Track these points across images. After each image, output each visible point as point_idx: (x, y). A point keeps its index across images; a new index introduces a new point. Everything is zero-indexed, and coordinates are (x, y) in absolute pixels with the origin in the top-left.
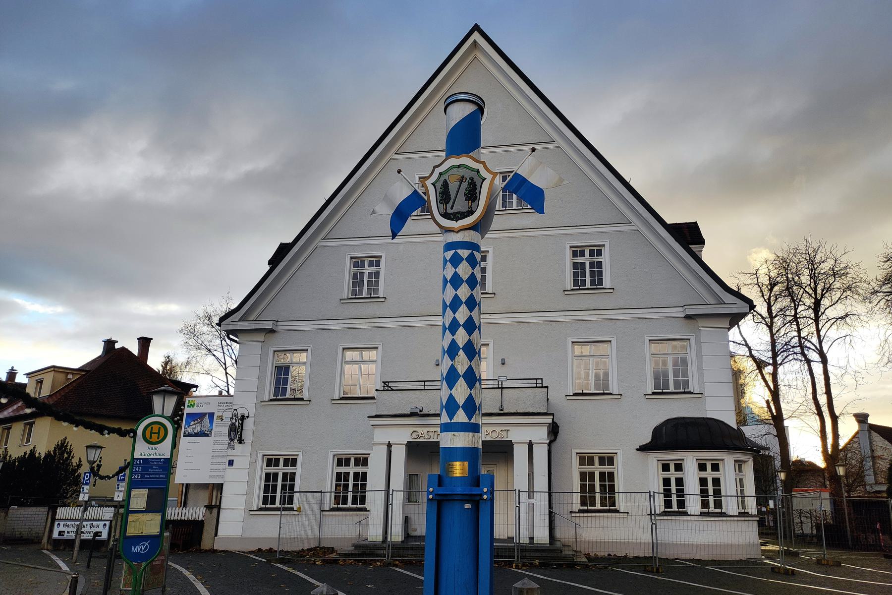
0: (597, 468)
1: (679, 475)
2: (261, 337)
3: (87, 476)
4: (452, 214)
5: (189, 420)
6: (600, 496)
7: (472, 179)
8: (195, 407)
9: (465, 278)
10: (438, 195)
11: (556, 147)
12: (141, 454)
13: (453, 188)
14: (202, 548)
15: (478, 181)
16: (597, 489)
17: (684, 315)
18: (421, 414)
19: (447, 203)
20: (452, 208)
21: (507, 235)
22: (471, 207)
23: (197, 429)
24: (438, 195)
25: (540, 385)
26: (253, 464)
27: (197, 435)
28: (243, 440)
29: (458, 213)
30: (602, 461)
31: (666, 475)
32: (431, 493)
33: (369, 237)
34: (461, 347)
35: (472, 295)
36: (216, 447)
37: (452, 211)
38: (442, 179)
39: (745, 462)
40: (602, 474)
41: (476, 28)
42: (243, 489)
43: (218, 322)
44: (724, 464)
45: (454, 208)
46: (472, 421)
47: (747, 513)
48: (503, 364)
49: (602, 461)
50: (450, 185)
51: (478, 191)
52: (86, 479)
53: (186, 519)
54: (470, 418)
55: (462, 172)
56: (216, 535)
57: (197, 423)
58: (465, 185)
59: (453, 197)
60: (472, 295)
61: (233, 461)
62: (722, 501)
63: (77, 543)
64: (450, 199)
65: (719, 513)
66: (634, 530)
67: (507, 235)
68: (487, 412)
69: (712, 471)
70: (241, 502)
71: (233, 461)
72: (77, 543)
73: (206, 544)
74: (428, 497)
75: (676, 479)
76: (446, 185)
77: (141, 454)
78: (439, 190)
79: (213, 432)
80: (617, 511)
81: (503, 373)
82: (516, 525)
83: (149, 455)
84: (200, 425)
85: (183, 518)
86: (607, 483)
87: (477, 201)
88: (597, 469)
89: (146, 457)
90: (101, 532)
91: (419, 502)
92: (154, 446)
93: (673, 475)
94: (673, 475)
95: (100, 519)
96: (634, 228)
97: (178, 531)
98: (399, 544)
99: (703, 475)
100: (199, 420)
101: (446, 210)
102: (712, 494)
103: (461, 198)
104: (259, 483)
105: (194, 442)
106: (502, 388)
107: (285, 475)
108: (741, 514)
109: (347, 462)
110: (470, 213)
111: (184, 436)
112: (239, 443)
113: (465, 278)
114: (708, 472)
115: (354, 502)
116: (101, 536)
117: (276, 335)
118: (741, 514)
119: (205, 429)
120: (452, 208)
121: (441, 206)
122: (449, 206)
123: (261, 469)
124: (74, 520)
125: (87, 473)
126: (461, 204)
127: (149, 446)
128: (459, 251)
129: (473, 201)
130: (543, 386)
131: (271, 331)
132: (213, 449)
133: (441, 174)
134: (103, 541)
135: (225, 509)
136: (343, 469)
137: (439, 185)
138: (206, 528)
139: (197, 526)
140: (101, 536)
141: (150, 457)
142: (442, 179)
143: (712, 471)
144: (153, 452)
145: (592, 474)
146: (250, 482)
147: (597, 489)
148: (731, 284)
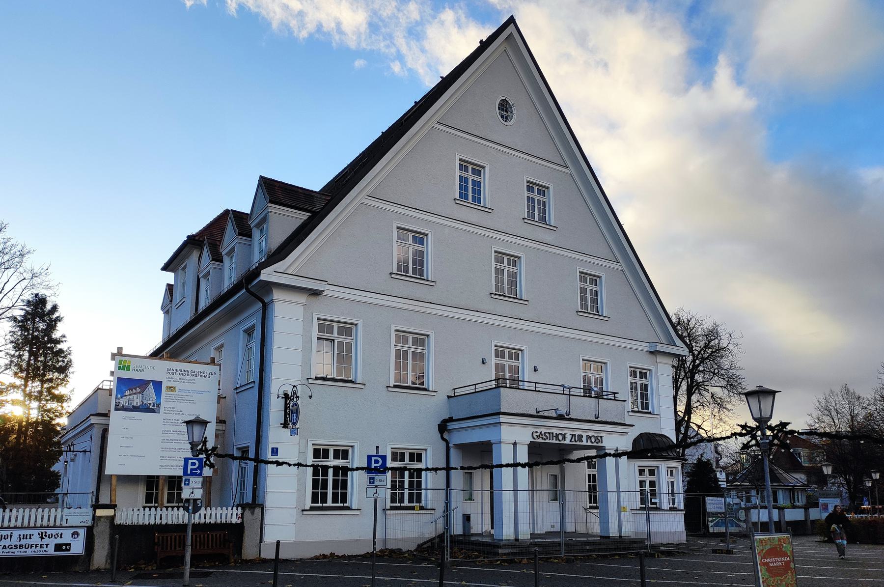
2: (302, 299)
5: (123, 388)
6: (409, 493)
8: (131, 369)
11: (567, 173)
14: (244, 557)
16: (406, 485)
17: (29, 263)
18: (538, 416)
21: (535, 246)
23: (137, 401)
27: (136, 409)
30: (412, 458)
31: (642, 478)
33: (507, 233)
36: (167, 428)
47: (676, 508)
48: (484, 363)
49: (337, 454)
52: (190, 467)
53: (213, 522)
56: (261, 541)
57: (136, 393)
62: (328, 493)
64: (74, 532)
65: (654, 508)
66: (678, 523)
67: (535, 246)
68: (587, 419)
71: (277, 449)
73: (249, 551)
75: (671, 482)
79: (162, 407)
80: (348, 508)
81: (535, 378)
82: (647, 521)
84: (140, 396)
85: (208, 521)
86: (415, 480)
88: (331, 462)
90: (70, 544)
91: (474, 500)
93: (647, 478)
94: (647, 478)
95: (58, 524)
96: (620, 268)
97: (206, 539)
98: (617, 539)
99: (642, 478)
100: (138, 390)
102: (489, 489)
105: (133, 418)
106: (570, 395)
108: (671, 509)
111: (116, 409)
112: (283, 427)
115: (335, 500)
116: (69, 550)
117: (319, 299)
118: (671, 509)
119: (149, 402)
124: (25, 528)
131: (315, 293)
132: (163, 431)
134: (75, 558)
135: (272, 509)
138: (247, 533)
139: (235, 532)
140: (69, 550)
145: (325, 468)
147: (406, 485)
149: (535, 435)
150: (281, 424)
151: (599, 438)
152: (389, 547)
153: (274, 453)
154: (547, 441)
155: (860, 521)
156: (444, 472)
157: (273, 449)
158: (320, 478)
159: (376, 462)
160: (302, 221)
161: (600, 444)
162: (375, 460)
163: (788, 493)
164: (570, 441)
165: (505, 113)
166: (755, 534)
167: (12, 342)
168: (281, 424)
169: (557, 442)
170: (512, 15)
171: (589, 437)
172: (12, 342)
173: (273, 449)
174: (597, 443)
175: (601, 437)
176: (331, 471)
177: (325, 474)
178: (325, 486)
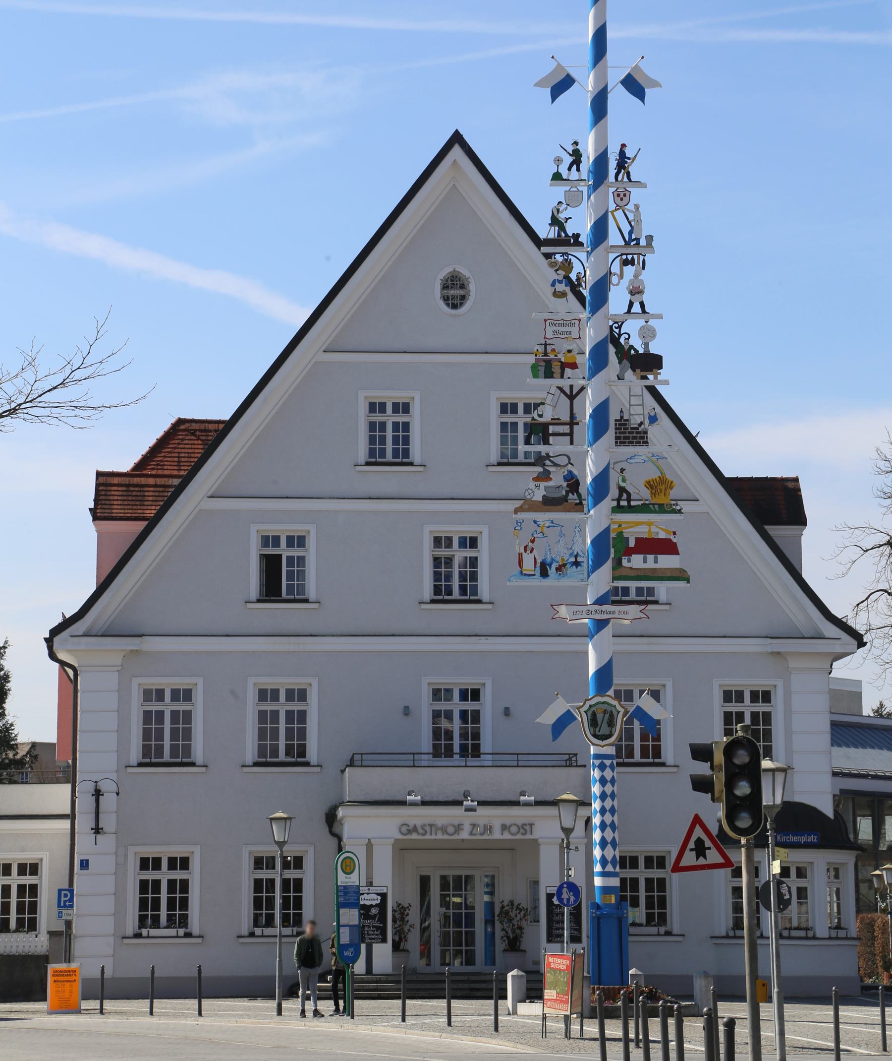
0: (642, 872)
1: (802, 883)
4: (599, 735)
7: (611, 712)
10: (589, 720)
13: (599, 717)
15: (615, 713)
19: (596, 727)
20: (599, 732)
22: (611, 732)
24: (589, 720)
25: (575, 764)
28: (102, 829)
29: (604, 735)
32: (594, 913)
34: (608, 824)
40: (172, 883)
41: (457, 139)
43: (48, 636)
44: (812, 870)
45: (601, 731)
50: (597, 715)
51: (615, 720)
52: (63, 899)
54: (615, 870)
55: (605, 707)
58: (607, 716)
59: (599, 723)
61: (87, 861)
63: (838, 902)
64: (598, 725)
69: (797, 878)
70: (108, 925)
71: (87, 861)
72: (838, 902)
74: (592, 915)
76: (594, 715)
83: (347, 883)
86: (656, 894)
87: (615, 728)
89: (345, 884)
92: (348, 876)
101: (595, 732)
102: (492, 1002)
103: (605, 725)
114: (791, 879)
120: (599, 732)
121: (591, 728)
122: (597, 730)
123: (134, 876)
125: (65, 890)
126: (605, 730)
127: (346, 875)
128: (604, 761)
130: (578, 765)
133: (591, 706)
137: (590, 713)
141: (347, 884)
143: (797, 878)
144: (348, 880)
145: (157, 884)
146: (119, 894)
148: (838, 613)
149: (404, 829)
150: (92, 829)
151: (528, 828)
152: (273, 1004)
153: (84, 866)
154: (428, 837)
156: (621, 1045)
157: (82, 861)
159: (66, 896)
160: (144, 526)
161: (528, 836)
162: (64, 894)
164: (471, 834)
166: (629, 1018)
167: (37, 761)
168: (103, 795)
169: (446, 837)
170: (457, 129)
171: (504, 828)
172: (37, 761)
174: (523, 834)
175: (531, 825)
177: (170, 918)
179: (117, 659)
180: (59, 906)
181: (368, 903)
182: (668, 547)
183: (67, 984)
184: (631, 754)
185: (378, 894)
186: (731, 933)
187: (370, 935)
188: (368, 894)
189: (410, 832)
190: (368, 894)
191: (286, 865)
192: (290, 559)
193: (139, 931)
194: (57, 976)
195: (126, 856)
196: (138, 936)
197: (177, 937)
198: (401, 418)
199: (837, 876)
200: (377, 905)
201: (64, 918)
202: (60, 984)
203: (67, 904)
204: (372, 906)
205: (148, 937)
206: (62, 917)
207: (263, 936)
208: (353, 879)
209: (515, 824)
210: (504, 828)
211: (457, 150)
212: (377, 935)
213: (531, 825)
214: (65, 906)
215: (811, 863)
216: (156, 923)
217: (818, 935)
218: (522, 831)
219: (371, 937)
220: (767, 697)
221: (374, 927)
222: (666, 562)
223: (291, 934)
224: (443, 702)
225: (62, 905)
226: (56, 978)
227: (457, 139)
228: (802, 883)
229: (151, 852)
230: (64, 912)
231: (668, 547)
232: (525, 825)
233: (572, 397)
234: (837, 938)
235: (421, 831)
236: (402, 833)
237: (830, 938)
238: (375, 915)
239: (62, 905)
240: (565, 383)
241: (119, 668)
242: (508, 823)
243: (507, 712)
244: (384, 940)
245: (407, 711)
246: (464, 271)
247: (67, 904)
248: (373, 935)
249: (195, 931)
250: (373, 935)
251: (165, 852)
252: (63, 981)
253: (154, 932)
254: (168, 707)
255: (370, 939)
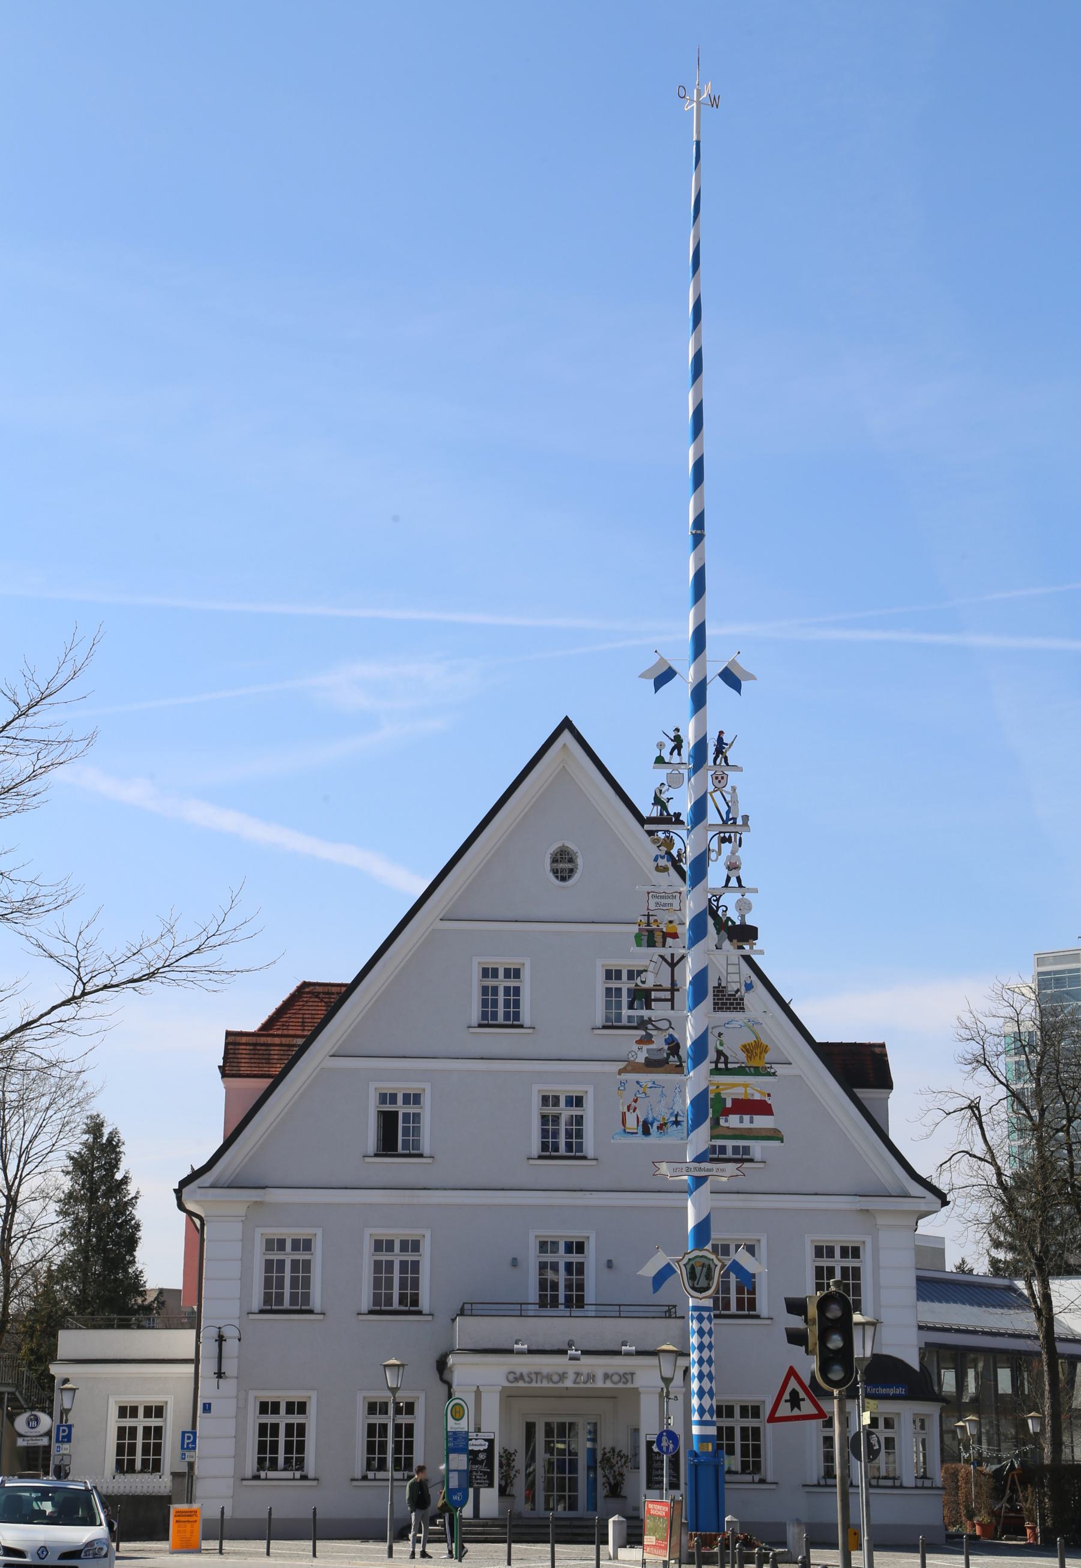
1: (889, 1433)
3: (189, 1438)
7: (709, 1265)
9: (706, 1344)
12: (451, 1428)
13: (698, 1270)
15: (712, 1266)
16: (390, 1446)
22: (709, 1284)
26: (241, 1410)
28: (224, 1373)
29: (702, 1288)
35: (702, 1342)
37: (698, 1286)
38: (691, 1263)
39: (928, 1415)
41: (566, 724)
42: (228, 1447)
46: (703, 1419)
49: (570, 1101)
52: (186, 1441)
55: (703, 1260)
58: (705, 1269)
59: (698, 1276)
60: (702, 1342)
61: (210, 1404)
62: (142, 1438)
70: (228, 1467)
71: (210, 1404)
76: (693, 1268)
77: (451, 1428)
78: (688, 1271)
92: (457, 1422)
103: (703, 1278)
104: (252, 1439)
107: (289, 1427)
109: (384, 1409)
110: (708, 1288)
113: (706, 1344)
122: (696, 1282)
123: (253, 1420)
125: (189, 1432)
126: (703, 1283)
129: (710, 1280)
136: (377, 1419)
137: (689, 1267)
142: (691, 1263)
145: (275, 1427)
146: (239, 1437)
147: (390, 1446)
150: (215, 1373)
151: (629, 1377)
152: (384, 1546)
154: (533, 1385)
155: (868, 1536)
157: (204, 1404)
158: (268, 1439)
159: (189, 1438)
161: (629, 1385)
163: (854, 1484)
165: (116, 1322)
169: (551, 1385)
170: (567, 717)
171: (607, 1376)
173: (204, 1404)
174: (624, 1383)
175: (632, 1374)
176: (138, 1465)
178: (289, 1447)
179: (242, 1210)
180: (182, 1448)
181: (476, 1448)
182: (762, 1108)
183: (189, 1525)
184: (727, 1306)
185: (485, 1440)
186: (822, 1482)
187: (476, 1479)
188: (476, 1439)
189: (516, 1380)
190: (476, 1439)
191: (398, 1411)
192: (406, 1116)
193: (257, 1473)
194: (179, 1516)
195: (246, 1400)
196: (256, 1478)
197: (294, 1479)
198: (296, 1419)
199: (923, 1427)
200: (484, 1451)
201: (187, 1459)
202: (181, 1524)
203: (190, 1446)
204: (479, 1451)
205: (266, 1479)
206: (184, 1459)
207: (375, 1480)
208: (462, 1425)
209: (617, 1373)
210: (607, 1376)
211: (566, 735)
212: (484, 1480)
213: (632, 1374)
214: (188, 1448)
215: (899, 1414)
216: (274, 1466)
217: (905, 1485)
218: (623, 1380)
219: (479, 1481)
220: (856, 1252)
221: (481, 1472)
222: (761, 1122)
223: (930, 1486)
224: (549, 1254)
225: (185, 1447)
226: (178, 1519)
227: (566, 724)
228: (889, 1433)
229: (270, 1396)
230: (187, 1454)
231: (762, 1108)
232: (626, 1373)
233: (673, 965)
234: (923, 1488)
235: (527, 1379)
236: (508, 1381)
237: (916, 1487)
238: (483, 1460)
239: (185, 1447)
240: (666, 952)
241: (243, 1218)
242: (610, 1371)
243: (610, 1264)
244: (491, 1485)
245: (515, 1263)
246: (572, 846)
247: (190, 1446)
248: (480, 1479)
249: (311, 1475)
250: (480, 1479)
251: (283, 1396)
252: (185, 1522)
253: (272, 1474)
254: (288, 1256)
255: (478, 1483)
